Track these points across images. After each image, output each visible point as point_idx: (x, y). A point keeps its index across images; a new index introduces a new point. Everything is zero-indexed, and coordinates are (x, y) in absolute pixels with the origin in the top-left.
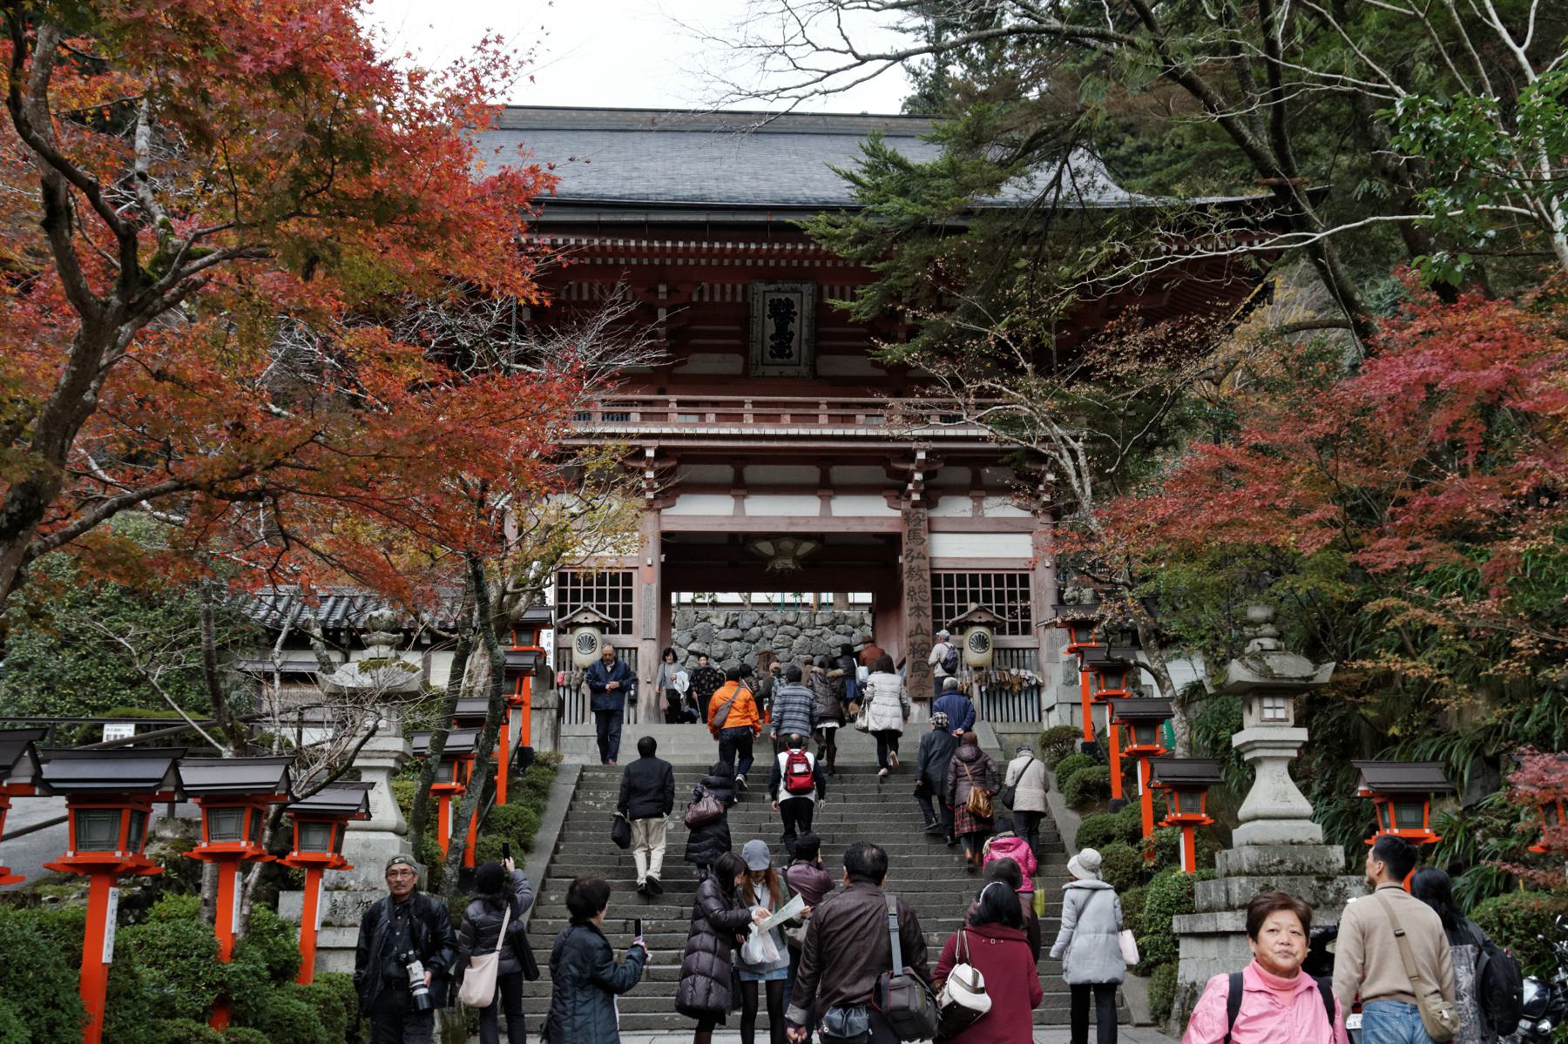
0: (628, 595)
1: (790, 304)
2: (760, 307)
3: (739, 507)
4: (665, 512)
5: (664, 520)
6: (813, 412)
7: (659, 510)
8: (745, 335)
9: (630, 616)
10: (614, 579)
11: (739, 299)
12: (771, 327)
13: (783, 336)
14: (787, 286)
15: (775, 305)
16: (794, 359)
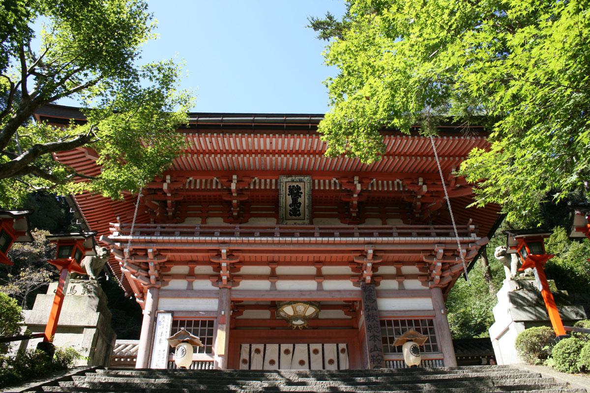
1: (299, 188)
2: (284, 190)
6: (312, 231)
8: (277, 212)
11: (273, 188)
12: (289, 200)
13: (295, 204)
14: (297, 178)
15: (291, 189)
16: (301, 216)
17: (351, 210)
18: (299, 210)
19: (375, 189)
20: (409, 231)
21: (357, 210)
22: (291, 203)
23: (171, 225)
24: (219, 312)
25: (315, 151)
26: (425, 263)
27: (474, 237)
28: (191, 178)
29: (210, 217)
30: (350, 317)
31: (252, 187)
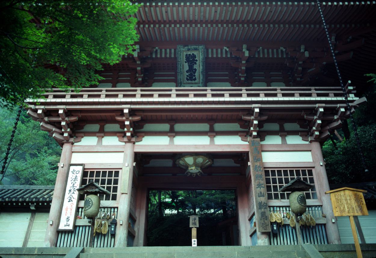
0: (116, 182)
1: (194, 56)
3: (172, 141)
4: (137, 144)
5: (136, 147)
7: (134, 143)
9: (116, 192)
10: (110, 173)
11: (173, 56)
12: (186, 67)
13: (192, 71)
16: (196, 81)
17: (296, 75)
18: (195, 76)
19: (261, 56)
20: (293, 92)
21: (245, 75)
22: (188, 69)
23: (332, 88)
24: (123, 164)
25: (239, 21)
26: (305, 120)
27: (351, 97)
28: (157, 48)
29: (119, 82)
30: (238, 165)
31: (154, 56)
